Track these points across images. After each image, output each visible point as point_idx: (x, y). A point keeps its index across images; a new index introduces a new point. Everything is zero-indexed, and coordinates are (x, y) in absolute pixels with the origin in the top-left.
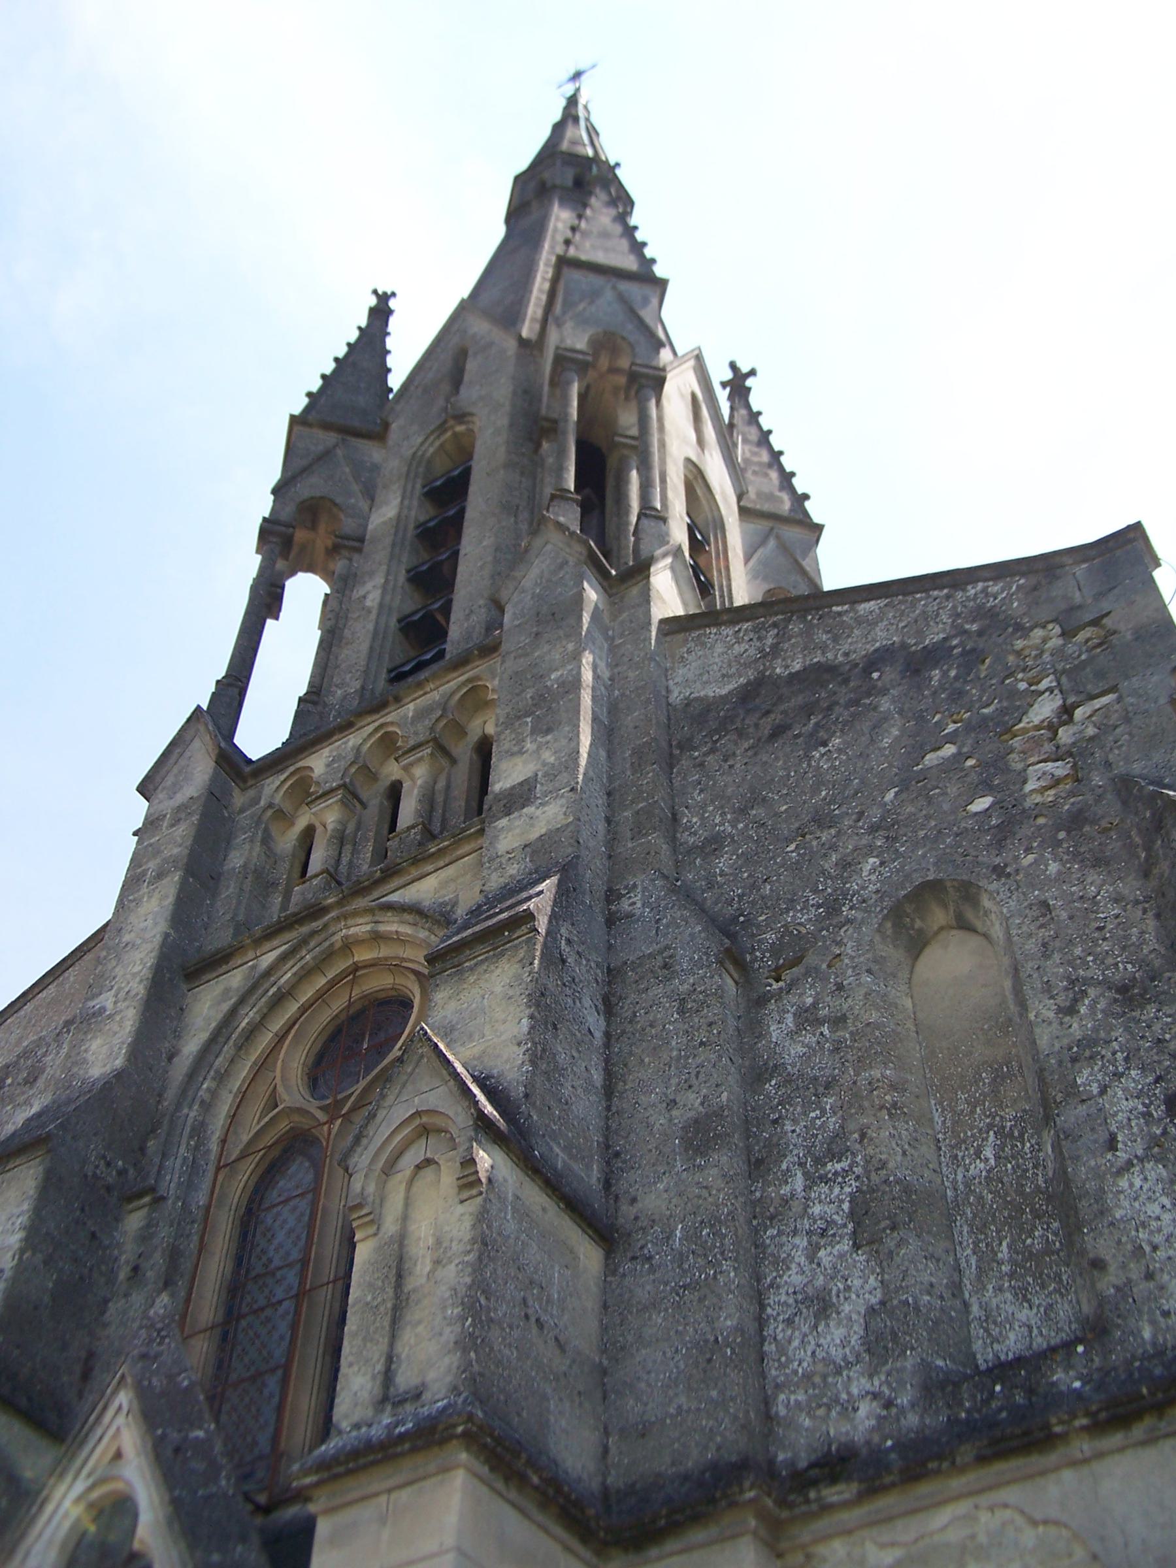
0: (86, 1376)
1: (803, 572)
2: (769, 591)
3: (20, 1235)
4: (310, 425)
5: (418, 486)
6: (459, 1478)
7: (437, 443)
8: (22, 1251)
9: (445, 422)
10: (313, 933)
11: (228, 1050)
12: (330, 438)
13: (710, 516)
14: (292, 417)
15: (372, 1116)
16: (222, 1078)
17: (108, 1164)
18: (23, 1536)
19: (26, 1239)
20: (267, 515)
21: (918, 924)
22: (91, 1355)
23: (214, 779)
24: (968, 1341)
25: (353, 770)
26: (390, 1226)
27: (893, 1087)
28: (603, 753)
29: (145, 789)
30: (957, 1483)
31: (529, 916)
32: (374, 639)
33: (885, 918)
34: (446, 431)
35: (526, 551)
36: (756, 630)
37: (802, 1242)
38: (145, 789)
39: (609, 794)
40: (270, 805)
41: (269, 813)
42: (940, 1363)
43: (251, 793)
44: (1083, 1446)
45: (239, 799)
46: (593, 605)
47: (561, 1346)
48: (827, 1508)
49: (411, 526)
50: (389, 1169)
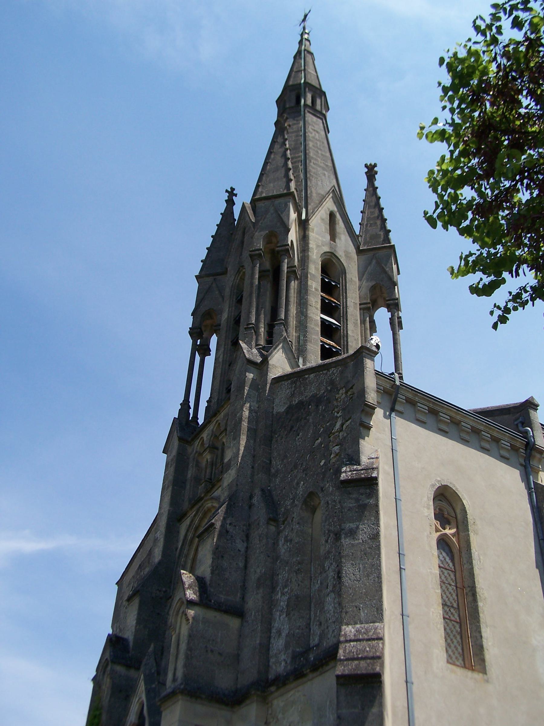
0: (162, 654)
1: (386, 272)
2: (372, 286)
3: (135, 622)
4: (203, 277)
5: (234, 299)
6: (180, 702)
7: (239, 278)
8: (136, 627)
9: (239, 269)
10: (200, 507)
11: (187, 547)
12: (210, 279)
13: (340, 269)
14: (197, 277)
15: (173, 599)
16: (187, 556)
17: (160, 591)
18: (129, 711)
19: (137, 623)
20: (191, 326)
21: (312, 504)
22: (163, 647)
23: (179, 446)
24: (309, 641)
25: (212, 439)
26: (177, 631)
27: (299, 563)
28: (252, 442)
29: (164, 452)
30: (292, 685)
31: (213, 524)
32: (221, 377)
33: (302, 504)
34: (240, 273)
35: (236, 358)
36: (291, 383)
37: (278, 613)
38: (164, 452)
39: (254, 457)
40: (196, 452)
41: (197, 455)
42: (298, 650)
43: (192, 447)
44: (311, 676)
45: (189, 449)
46: (250, 381)
47: (220, 654)
48: (272, 693)
49: (232, 320)
50: (177, 614)
